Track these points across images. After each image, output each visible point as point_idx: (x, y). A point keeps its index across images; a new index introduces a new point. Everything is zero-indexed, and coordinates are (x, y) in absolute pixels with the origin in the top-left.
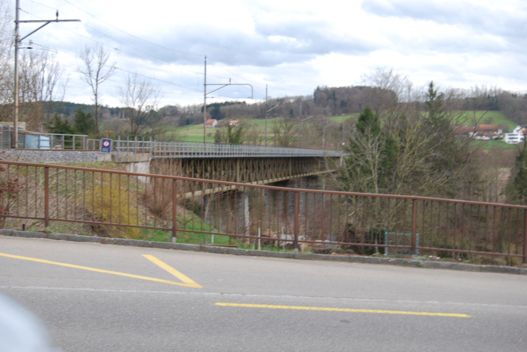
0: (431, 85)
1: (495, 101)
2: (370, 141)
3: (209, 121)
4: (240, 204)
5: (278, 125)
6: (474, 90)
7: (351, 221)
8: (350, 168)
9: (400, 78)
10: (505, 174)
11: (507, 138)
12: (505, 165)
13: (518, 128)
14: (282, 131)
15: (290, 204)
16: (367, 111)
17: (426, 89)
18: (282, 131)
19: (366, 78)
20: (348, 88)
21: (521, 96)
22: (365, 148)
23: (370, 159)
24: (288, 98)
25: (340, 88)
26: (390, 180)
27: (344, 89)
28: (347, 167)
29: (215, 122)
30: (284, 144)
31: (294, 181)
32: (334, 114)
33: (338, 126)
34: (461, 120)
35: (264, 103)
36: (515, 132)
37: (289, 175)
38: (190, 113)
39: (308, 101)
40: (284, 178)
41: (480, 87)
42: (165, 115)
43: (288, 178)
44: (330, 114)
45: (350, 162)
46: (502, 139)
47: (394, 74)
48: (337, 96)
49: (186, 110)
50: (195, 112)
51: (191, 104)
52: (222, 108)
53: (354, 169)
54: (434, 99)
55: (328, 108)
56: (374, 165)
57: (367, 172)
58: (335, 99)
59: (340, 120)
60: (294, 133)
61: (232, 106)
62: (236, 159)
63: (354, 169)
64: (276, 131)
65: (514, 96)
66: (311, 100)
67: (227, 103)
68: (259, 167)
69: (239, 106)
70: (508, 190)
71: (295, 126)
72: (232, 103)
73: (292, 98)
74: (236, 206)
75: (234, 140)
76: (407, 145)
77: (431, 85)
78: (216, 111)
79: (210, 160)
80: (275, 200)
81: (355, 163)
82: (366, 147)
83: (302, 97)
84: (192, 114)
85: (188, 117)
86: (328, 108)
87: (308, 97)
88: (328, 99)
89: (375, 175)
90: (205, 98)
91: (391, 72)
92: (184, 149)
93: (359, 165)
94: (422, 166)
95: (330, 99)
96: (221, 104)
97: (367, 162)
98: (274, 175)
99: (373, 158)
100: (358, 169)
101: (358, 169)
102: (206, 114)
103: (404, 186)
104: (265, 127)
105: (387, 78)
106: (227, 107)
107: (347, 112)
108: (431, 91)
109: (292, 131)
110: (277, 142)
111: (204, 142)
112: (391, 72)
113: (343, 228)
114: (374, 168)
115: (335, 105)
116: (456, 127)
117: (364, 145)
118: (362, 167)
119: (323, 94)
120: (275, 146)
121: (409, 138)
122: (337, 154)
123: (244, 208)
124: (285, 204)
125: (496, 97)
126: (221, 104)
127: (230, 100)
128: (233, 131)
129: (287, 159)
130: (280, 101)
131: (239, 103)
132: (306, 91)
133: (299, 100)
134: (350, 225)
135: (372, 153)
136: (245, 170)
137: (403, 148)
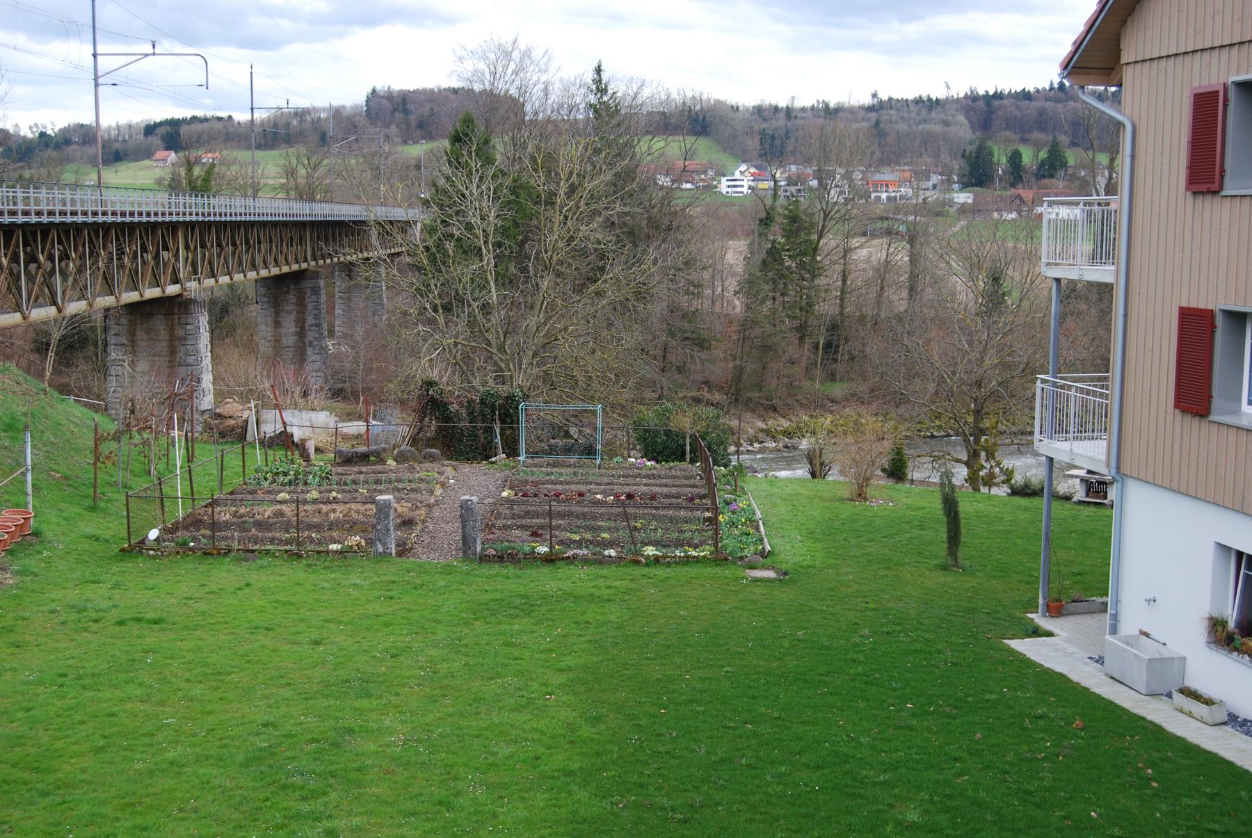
0: (598, 70)
1: (701, 118)
2: (476, 180)
3: (160, 154)
4: (188, 327)
5: (294, 162)
6: (663, 97)
7: (434, 375)
8: (430, 243)
9: (533, 54)
10: (735, 254)
11: (724, 186)
12: (732, 235)
13: (743, 167)
14: (302, 172)
15: (310, 320)
16: (468, 121)
17: (589, 76)
18: (302, 172)
19: (464, 53)
20: (432, 91)
21: (747, 110)
22: (463, 195)
23: (475, 221)
24: (315, 110)
25: (414, 92)
26: (524, 270)
27: (424, 92)
28: (424, 241)
29: (172, 156)
30: (306, 194)
31: (317, 272)
32: (405, 142)
33: (413, 162)
34: (652, 148)
35: (269, 119)
36: (737, 175)
37: (306, 260)
38: (120, 139)
39: (354, 115)
40: (295, 267)
41: (674, 95)
42: (68, 142)
43: (304, 266)
44: (398, 140)
45: (430, 230)
46: (716, 187)
47: (522, 46)
48: (411, 107)
49: (113, 133)
50: (130, 136)
51: (123, 121)
52: (184, 130)
53: (439, 246)
54: (605, 99)
55: (393, 129)
56: (486, 236)
57: (470, 251)
58: (406, 112)
59: (416, 150)
60: (325, 177)
61: (205, 124)
62: (174, 226)
63: (439, 246)
64: (290, 173)
65: (736, 109)
66: (360, 115)
67: (194, 118)
68: (234, 244)
69: (219, 125)
70: (749, 287)
71: (326, 162)
72: (206, 120)
73: (324, 110)
74: (180, 332)
75: (200, 187)
76: (563, 188)
77: (598, 70)
78: (171, 135)
79: (151, 228)
80: (277, 313)
81: (442, 230)
82: (467, 193)
83: (343, 107)
84: (125, 141)
85: (117, 146)
86: (393, 129)
87: (355, 107)
88: (393, 111)
89: (489, 259)
90: (97, 85)
91: (515, 42)
92: (69, 204)
93: (452, 235)
94: (598, 236)
95: (395, 112)
96: (184, 120)
97: (469, 227)
98: (270, 260)
99: (483, 219)
100: (450, 246)
101: (450, 246)
102: (155, 140)
103: (558, 284)
104: (271, 166)
105: (508, 55)
106: (197, 127)
107: (430, 137)
108: (598, 81)
109: (321, 171)
110: (293, 194)
111: (99, 186)
112: (515, 42)
113: (415, 389)
114: (485, 243)
115: (408, 124)
116: (649, 158)
117: (463, 189)
118: (459, 240)
119: (384, 101)
120: (288, 199)
121: (567, 171)
122: (399, 214)
123: (196, 334)
124: (301, 323)
125: (702, 108)
126: (184, 121)
127: (200, 113)
128: (197, 171)
129: (300, 226)
130: (301, 114)
131: (220, 119)
132: (350, 94)
133: (337, 113)
134: (430, 384)
135: (483, 212)
136: (215, 250)
137: (553, 194)
